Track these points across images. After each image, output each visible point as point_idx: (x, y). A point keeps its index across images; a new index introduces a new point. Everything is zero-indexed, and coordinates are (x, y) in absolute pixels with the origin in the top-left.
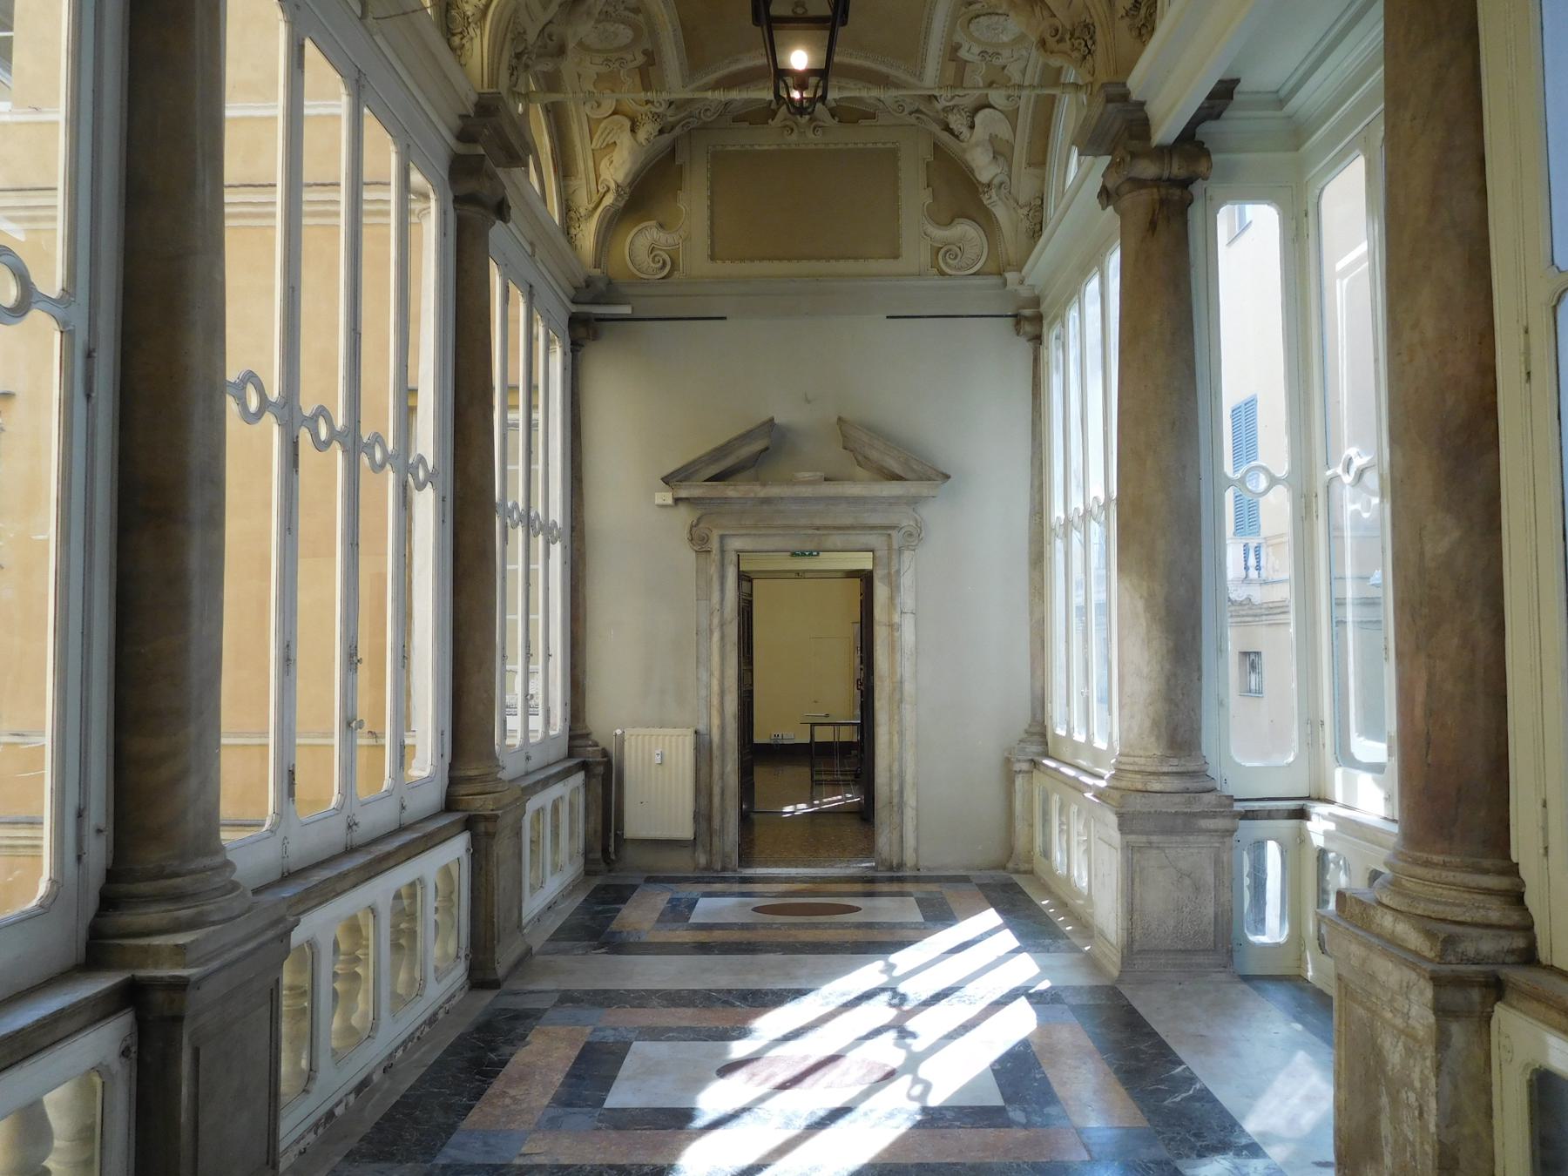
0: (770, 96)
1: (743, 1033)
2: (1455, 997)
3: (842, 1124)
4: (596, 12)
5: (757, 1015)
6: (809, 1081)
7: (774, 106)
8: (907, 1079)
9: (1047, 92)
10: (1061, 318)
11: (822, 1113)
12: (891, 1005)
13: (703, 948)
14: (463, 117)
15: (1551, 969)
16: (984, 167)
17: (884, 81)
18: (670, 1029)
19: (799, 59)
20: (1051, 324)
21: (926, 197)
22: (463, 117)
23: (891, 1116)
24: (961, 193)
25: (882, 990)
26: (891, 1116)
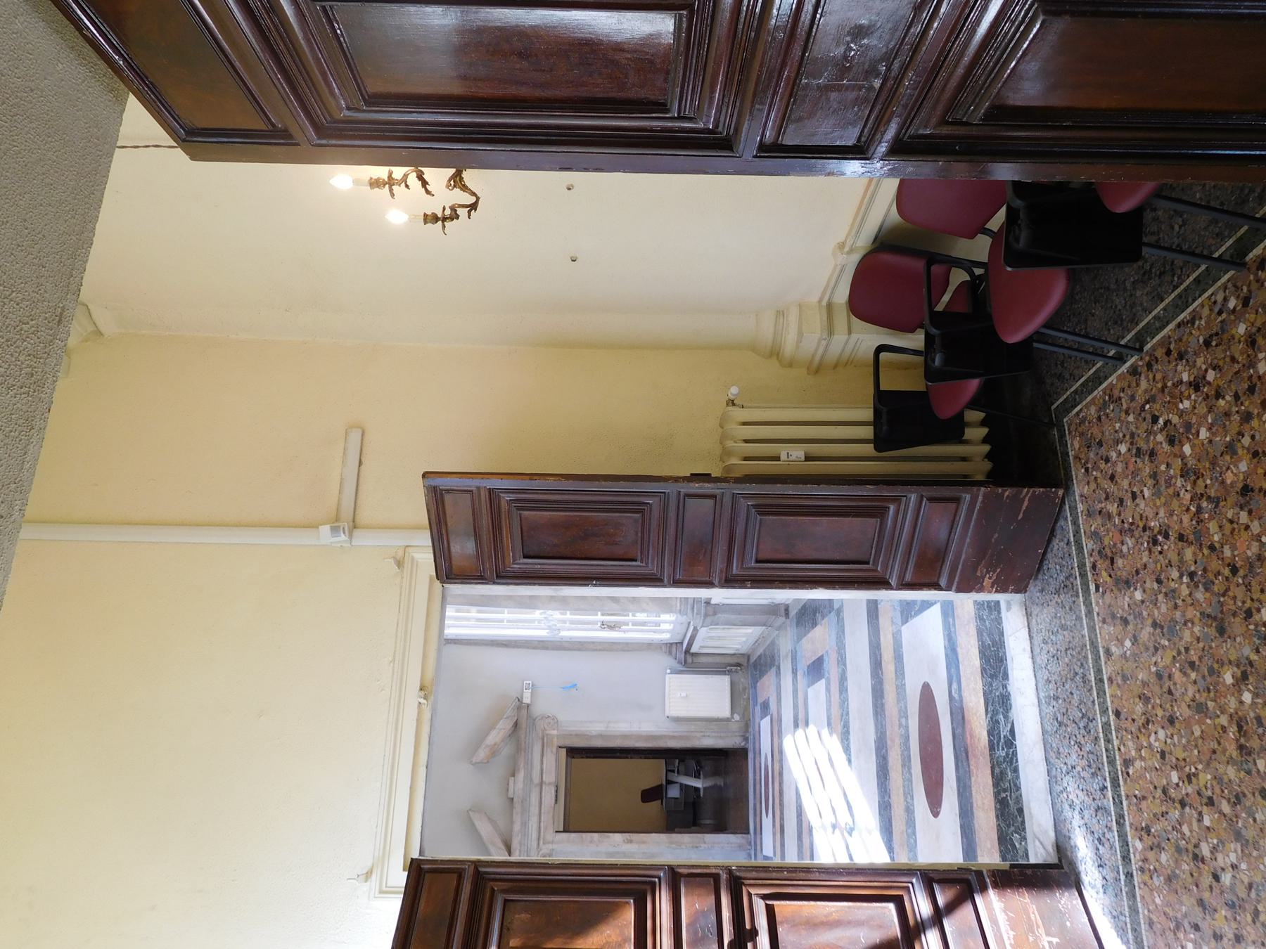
1: (831, 734)
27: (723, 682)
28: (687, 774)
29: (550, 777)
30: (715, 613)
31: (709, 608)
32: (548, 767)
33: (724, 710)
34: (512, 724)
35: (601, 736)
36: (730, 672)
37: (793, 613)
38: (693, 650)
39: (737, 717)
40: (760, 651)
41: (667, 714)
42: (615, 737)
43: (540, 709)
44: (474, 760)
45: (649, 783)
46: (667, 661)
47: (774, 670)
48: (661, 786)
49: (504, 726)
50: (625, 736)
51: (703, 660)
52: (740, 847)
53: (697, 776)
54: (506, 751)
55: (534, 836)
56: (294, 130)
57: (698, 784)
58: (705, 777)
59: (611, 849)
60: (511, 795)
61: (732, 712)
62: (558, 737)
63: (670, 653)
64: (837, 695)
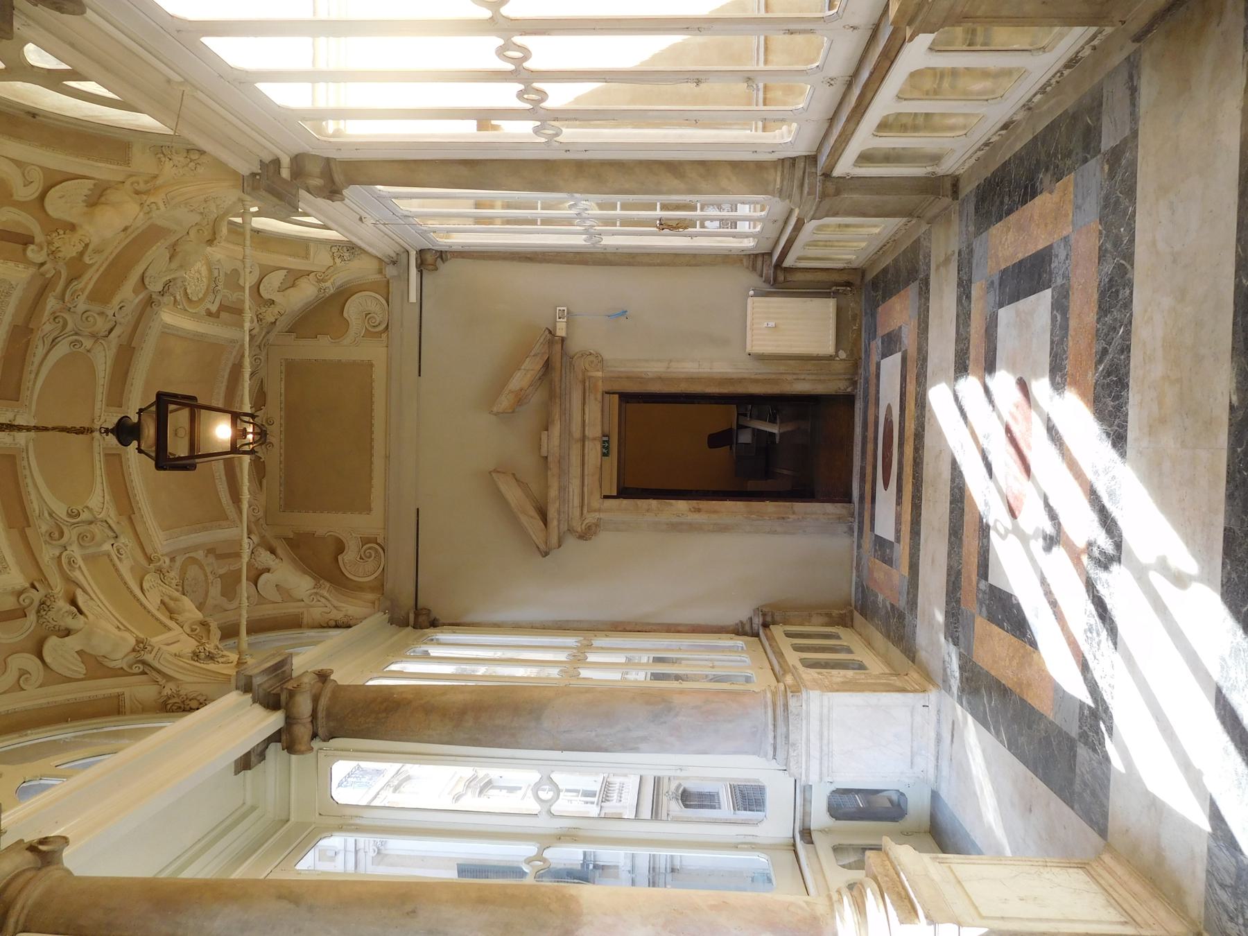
1: (1058, 386)
3: (984, 471)
4: (177, 594)
5: (1083, 395)
6: (1012, 450)
9: (248, 237)
10: (424, 234)
11: (990, 458)
12: (1090, 545)
13: (915, 532)
14: (254, 702)
16: (306, 292)
18: (1066, 319)
19: (222, 431)
21: (324, 341)
22: (254, 702)
23: (986, 504)
24: (325, 313)
25: (1118, 546)
26: (986, 504)
27: (825, 309)
28: (760, 418)
29: (594, 431)
30: (838, 192)
31: (829, 184)
32: (591, 418)
33: (826, 345)
35: (660, 379)
36: (835, 294)
37: (967, 189)
38: (788, 262)
39: (842, 355)
40: (887, 261)
41: (749, 349)
42: (679, 380)
43: (578, 343)
44: (495, 409)
46: (753, 280)
47: (913, 289)
48: (730, 430)
49: (532, 367)
50: (691, 379)
51: (799, 277)
52: (840, 519)
53: (773, 421)
54: (536, 398)
55: (577, 502)
56: (866, 663)
57: (774, 429)
58: (782, 422)
60: (544, 453)
61: (837, 350)
62: (604, 379)
63: (754, 268)
64: (1091, 317)
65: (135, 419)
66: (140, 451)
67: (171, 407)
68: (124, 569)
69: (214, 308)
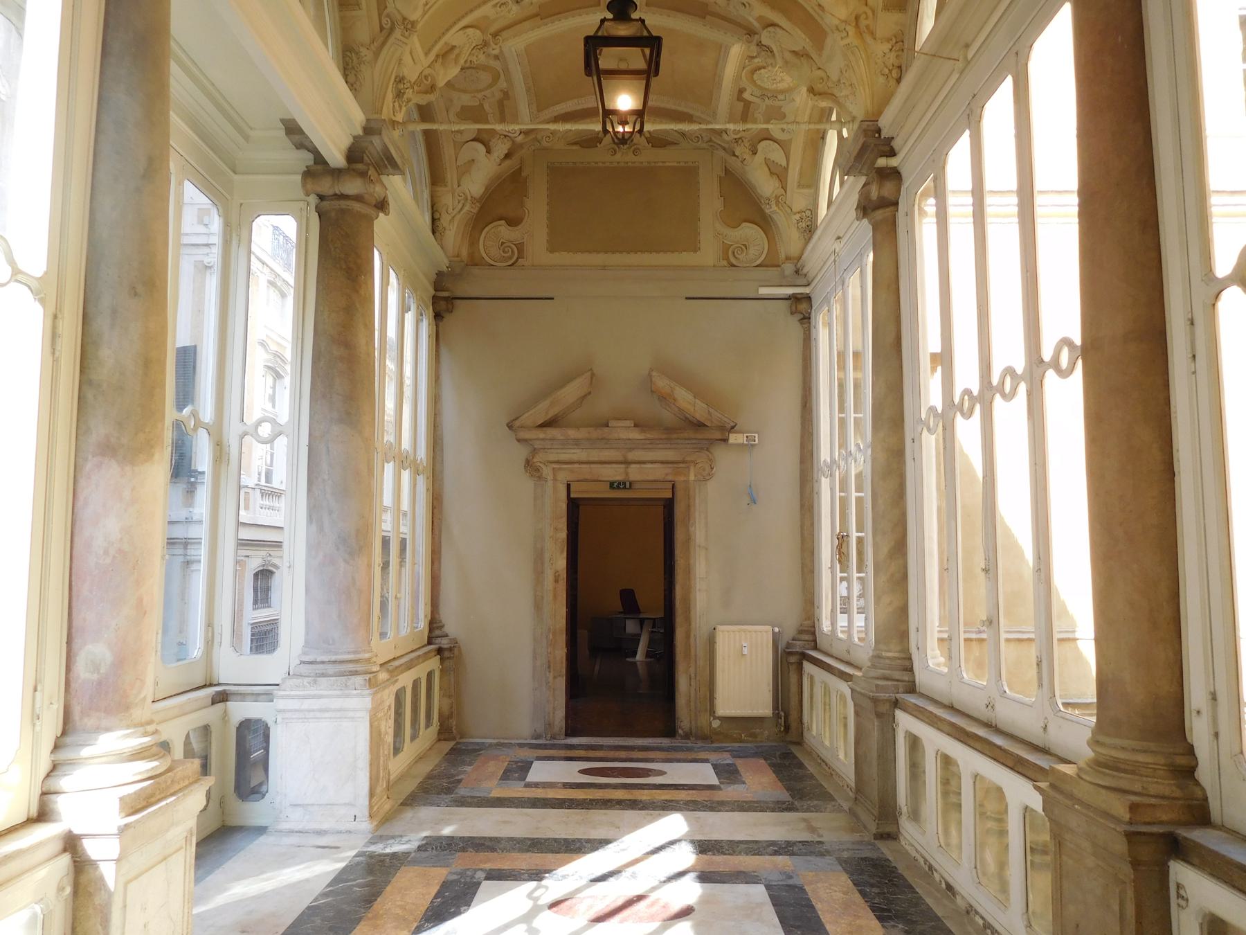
0: (599, 127)
2: (1038, 859)
4: (462, 62)
6: (620, 902)
7: (601, 135)
8: (540, 902)
9: (818, 127)
11: (611, 879)
13: (535, 803)
15: (1222, 828)
16: (765, 185)
17: (688, 118)
19: (625, 101)
20: (821, 305)
21: (718, 204)
23: (564, 877)
24: (746, 205)
27: (761, 705)
28: (651, 642)
29: (635, 473)
30: (879, 715)
31: (887, 706)
32: (648, 470)
34: (702, 420)
35: (688, 539)
36: (776, 715)
37: (886, 849)
38: (808, 667)
39: (716, 724)
40: (811, 768)
41: (720, 628)
43: (724, 459)
44: (654, 374)
45: (642, 600)
47: (784, 795)
48: (638, 611)
49: (698, 410)
50: (689, 571)
51: (793, 678)
52: (549, 725)
53: (648, 655)
54: (667, 416)
55: (563, 457)
56: (401, 755)
57: (640, 656)
59: (547, 556)
62: (687, 482)
63: (801, 632)
65: (635, 16)
66: (603, 21)
67: (647, 51)
68: (486, 10)
69: (746, 96)
